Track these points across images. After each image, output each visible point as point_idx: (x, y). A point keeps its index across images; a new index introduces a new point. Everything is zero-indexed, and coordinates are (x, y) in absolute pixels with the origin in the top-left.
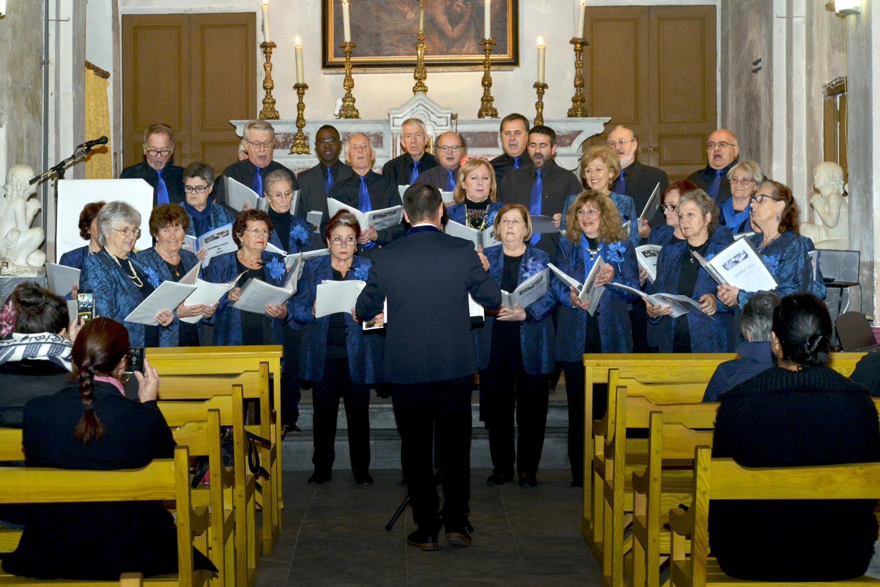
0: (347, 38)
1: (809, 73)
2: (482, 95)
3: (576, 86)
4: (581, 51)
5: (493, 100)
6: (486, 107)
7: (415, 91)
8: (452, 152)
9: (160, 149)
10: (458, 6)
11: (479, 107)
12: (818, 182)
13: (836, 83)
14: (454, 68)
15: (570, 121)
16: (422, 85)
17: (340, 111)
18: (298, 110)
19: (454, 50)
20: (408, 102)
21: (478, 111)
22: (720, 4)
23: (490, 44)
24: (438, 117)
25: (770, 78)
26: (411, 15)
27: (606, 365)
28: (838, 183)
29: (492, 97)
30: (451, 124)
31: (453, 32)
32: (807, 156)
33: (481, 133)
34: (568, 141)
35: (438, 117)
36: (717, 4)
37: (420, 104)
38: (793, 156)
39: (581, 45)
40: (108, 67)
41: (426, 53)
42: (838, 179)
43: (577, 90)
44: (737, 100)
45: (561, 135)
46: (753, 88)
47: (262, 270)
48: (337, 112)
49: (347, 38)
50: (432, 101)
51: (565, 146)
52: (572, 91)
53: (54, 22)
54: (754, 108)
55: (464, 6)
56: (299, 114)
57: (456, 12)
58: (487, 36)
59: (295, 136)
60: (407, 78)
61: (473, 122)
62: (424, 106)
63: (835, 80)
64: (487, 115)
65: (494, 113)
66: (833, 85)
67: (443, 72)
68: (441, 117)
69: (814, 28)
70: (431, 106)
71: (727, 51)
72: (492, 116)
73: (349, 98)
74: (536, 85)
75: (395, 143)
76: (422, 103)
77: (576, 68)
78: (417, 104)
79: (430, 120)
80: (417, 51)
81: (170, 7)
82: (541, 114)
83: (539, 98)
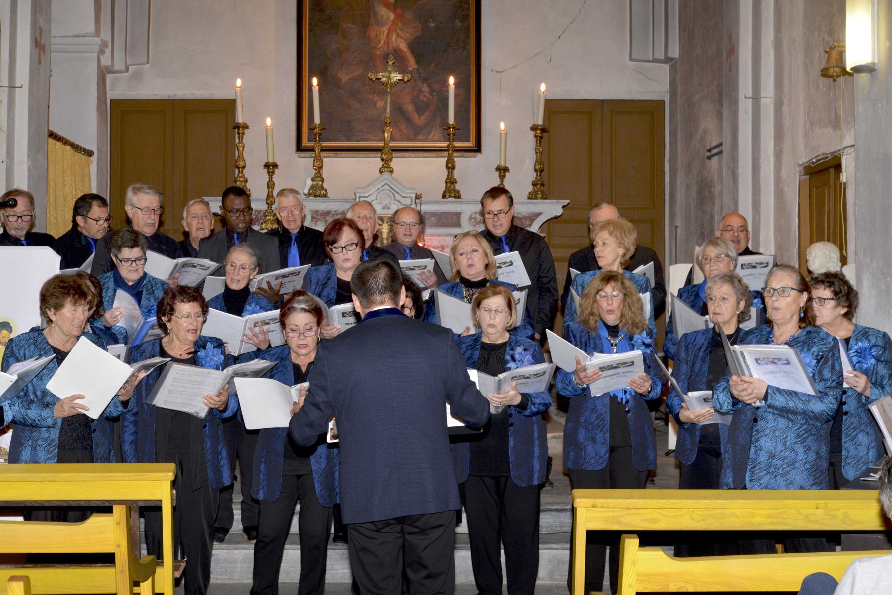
0: (317, 120)
1: (778, 154)
2: (446, 177)
3: (536, 170)
4: (541, 137)
5: (456, 182)
6: (450, 189)
7: (381, 172)
8: (410, 229)
9: (21, 213)
10: (425, 96)
11: (444, 189)
12: (813, 264)
13: (817, 161)
14: (421, 154)
15: (531, 203)
16: (389, 167)
17: (309, 190)
18: (268, 187)
19: (420, 137)
20: (374, 182)
21: (442, 192)
22: (668, 99)
23: (454, 128)
24: (403, 197)
25: (734, 159)
26: (380, 104)
27: (605, 506)
28: (835, 264)
29: (455, 179)
30: (416, 204)
32: (775, 238)
33: (445, 213)
35: (403, 197)
36: (665, 100)
37: (386, 184)
38: (760, 238)
39: (542, 132)
40: (92, 146)
41: (392, 139)
42: (835, 261)
43: (537, 175)
44: (688, 186)
45: (521, 216)
46: (706, 174)
47: (193, 358)
48: (306, 191)
49: (317, 120)
50: (397, 181)
52: (532, 176)
53: (7, 89)
54: (706, 193)
55: (431, 97)
56: (268, 192)
58: (452, 121)
59: (264, 213)
60: (374, 162)
61: (436, 203)
62: (389, 186)
63: (816, 157)
64: (450, 196)
65: (457, 195)
66: (813, 163)
67: (410, 157)
68: (406, 197)
69: (785, 108)
70: (396, 186)
71: (676, 143)
72: (456, 197)
73: (317, 177)
74: (498, 169)
76: (388, 182)
77: (536, 153)
78: (383, 183)
79: (395, 200)
80: (384, 134)
83: (500, 181)
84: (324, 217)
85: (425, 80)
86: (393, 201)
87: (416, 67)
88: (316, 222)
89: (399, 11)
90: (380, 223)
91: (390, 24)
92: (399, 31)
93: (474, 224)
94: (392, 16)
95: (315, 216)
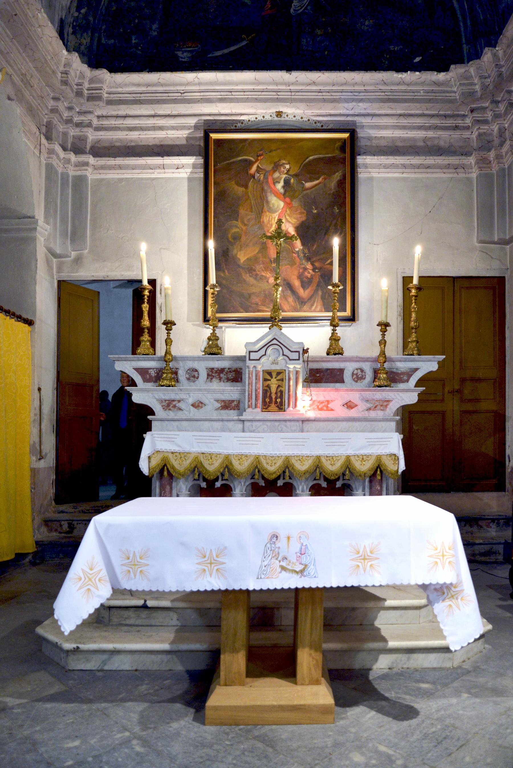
5: (339, 340)
10: (309, 273)
31: (303, 293)
33: (329, 369)
34: (405, 378)
51: (403, 382)
56: (166, 350)
57: (307, 278)
75: (251, 376)
81: (93, 274)
82: (384, 351)
84: (219, 375)
85: (308, 259)
86: (281, 357)
87: (302, 248)
88: (212, 379)
89: (288, 200)
90: (268, 377)
91: (280, 211)
92: (288, 217)
93: (356, 379)
94: (282, 204)
95: (211, 373)
